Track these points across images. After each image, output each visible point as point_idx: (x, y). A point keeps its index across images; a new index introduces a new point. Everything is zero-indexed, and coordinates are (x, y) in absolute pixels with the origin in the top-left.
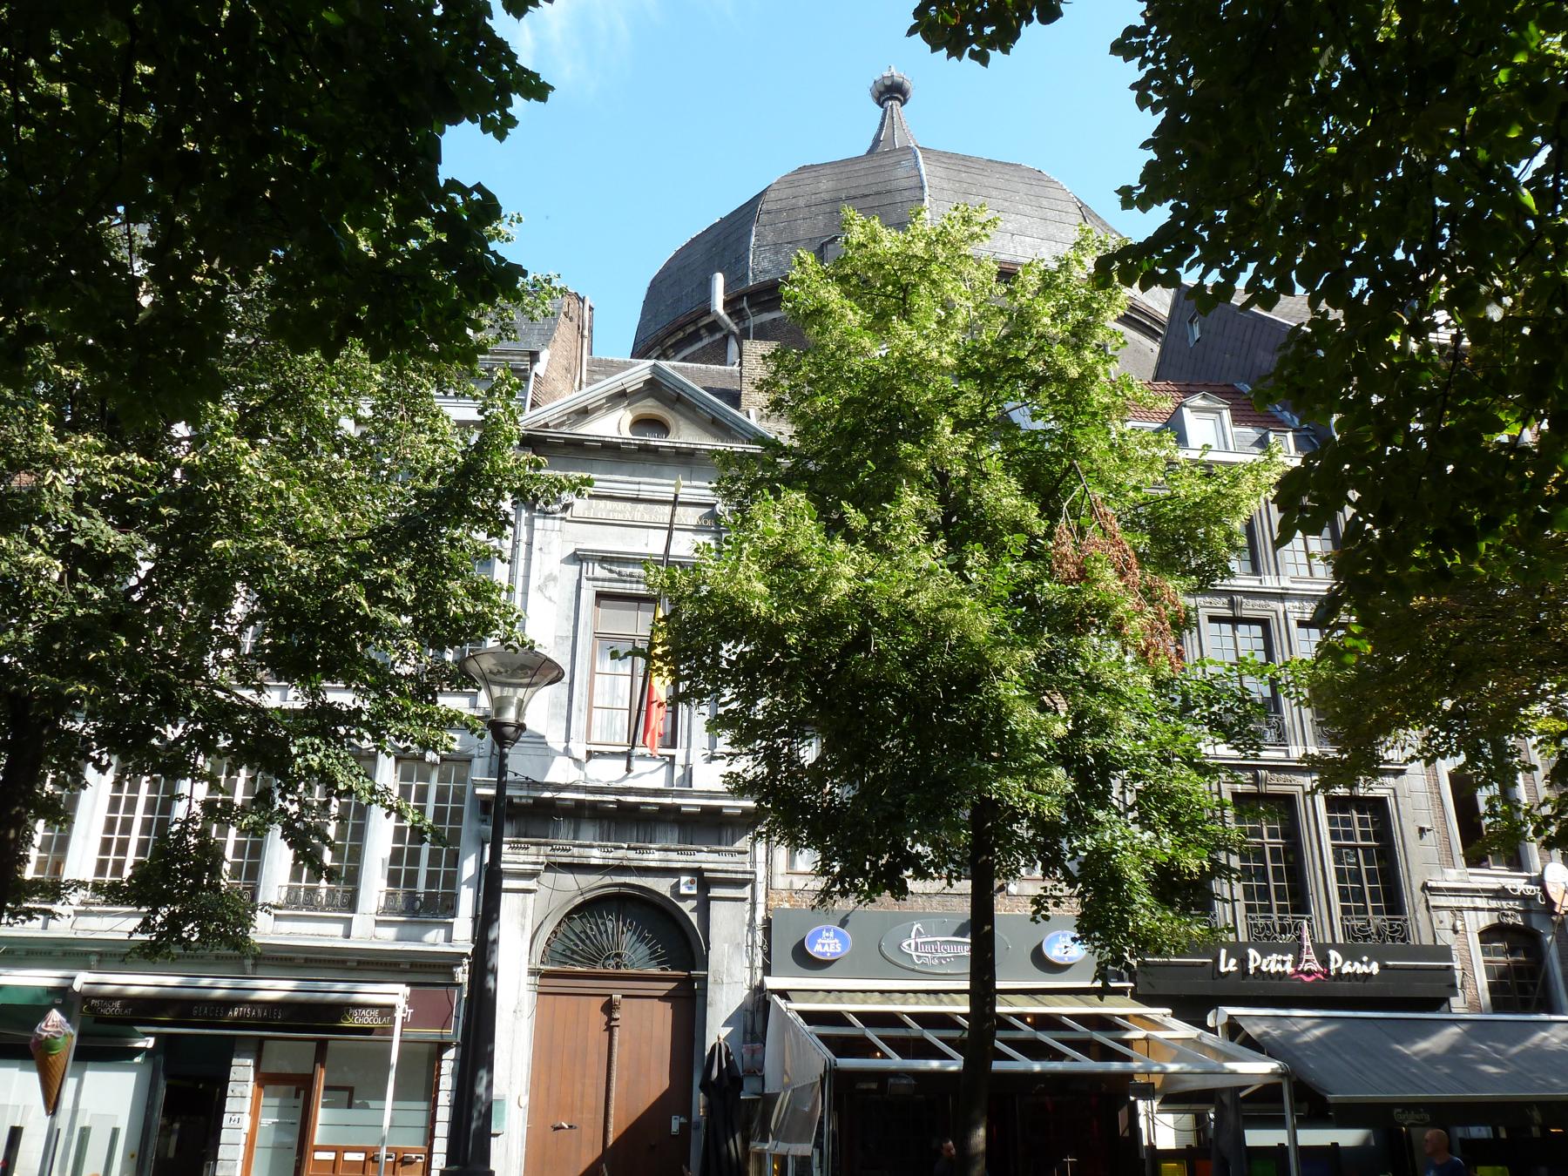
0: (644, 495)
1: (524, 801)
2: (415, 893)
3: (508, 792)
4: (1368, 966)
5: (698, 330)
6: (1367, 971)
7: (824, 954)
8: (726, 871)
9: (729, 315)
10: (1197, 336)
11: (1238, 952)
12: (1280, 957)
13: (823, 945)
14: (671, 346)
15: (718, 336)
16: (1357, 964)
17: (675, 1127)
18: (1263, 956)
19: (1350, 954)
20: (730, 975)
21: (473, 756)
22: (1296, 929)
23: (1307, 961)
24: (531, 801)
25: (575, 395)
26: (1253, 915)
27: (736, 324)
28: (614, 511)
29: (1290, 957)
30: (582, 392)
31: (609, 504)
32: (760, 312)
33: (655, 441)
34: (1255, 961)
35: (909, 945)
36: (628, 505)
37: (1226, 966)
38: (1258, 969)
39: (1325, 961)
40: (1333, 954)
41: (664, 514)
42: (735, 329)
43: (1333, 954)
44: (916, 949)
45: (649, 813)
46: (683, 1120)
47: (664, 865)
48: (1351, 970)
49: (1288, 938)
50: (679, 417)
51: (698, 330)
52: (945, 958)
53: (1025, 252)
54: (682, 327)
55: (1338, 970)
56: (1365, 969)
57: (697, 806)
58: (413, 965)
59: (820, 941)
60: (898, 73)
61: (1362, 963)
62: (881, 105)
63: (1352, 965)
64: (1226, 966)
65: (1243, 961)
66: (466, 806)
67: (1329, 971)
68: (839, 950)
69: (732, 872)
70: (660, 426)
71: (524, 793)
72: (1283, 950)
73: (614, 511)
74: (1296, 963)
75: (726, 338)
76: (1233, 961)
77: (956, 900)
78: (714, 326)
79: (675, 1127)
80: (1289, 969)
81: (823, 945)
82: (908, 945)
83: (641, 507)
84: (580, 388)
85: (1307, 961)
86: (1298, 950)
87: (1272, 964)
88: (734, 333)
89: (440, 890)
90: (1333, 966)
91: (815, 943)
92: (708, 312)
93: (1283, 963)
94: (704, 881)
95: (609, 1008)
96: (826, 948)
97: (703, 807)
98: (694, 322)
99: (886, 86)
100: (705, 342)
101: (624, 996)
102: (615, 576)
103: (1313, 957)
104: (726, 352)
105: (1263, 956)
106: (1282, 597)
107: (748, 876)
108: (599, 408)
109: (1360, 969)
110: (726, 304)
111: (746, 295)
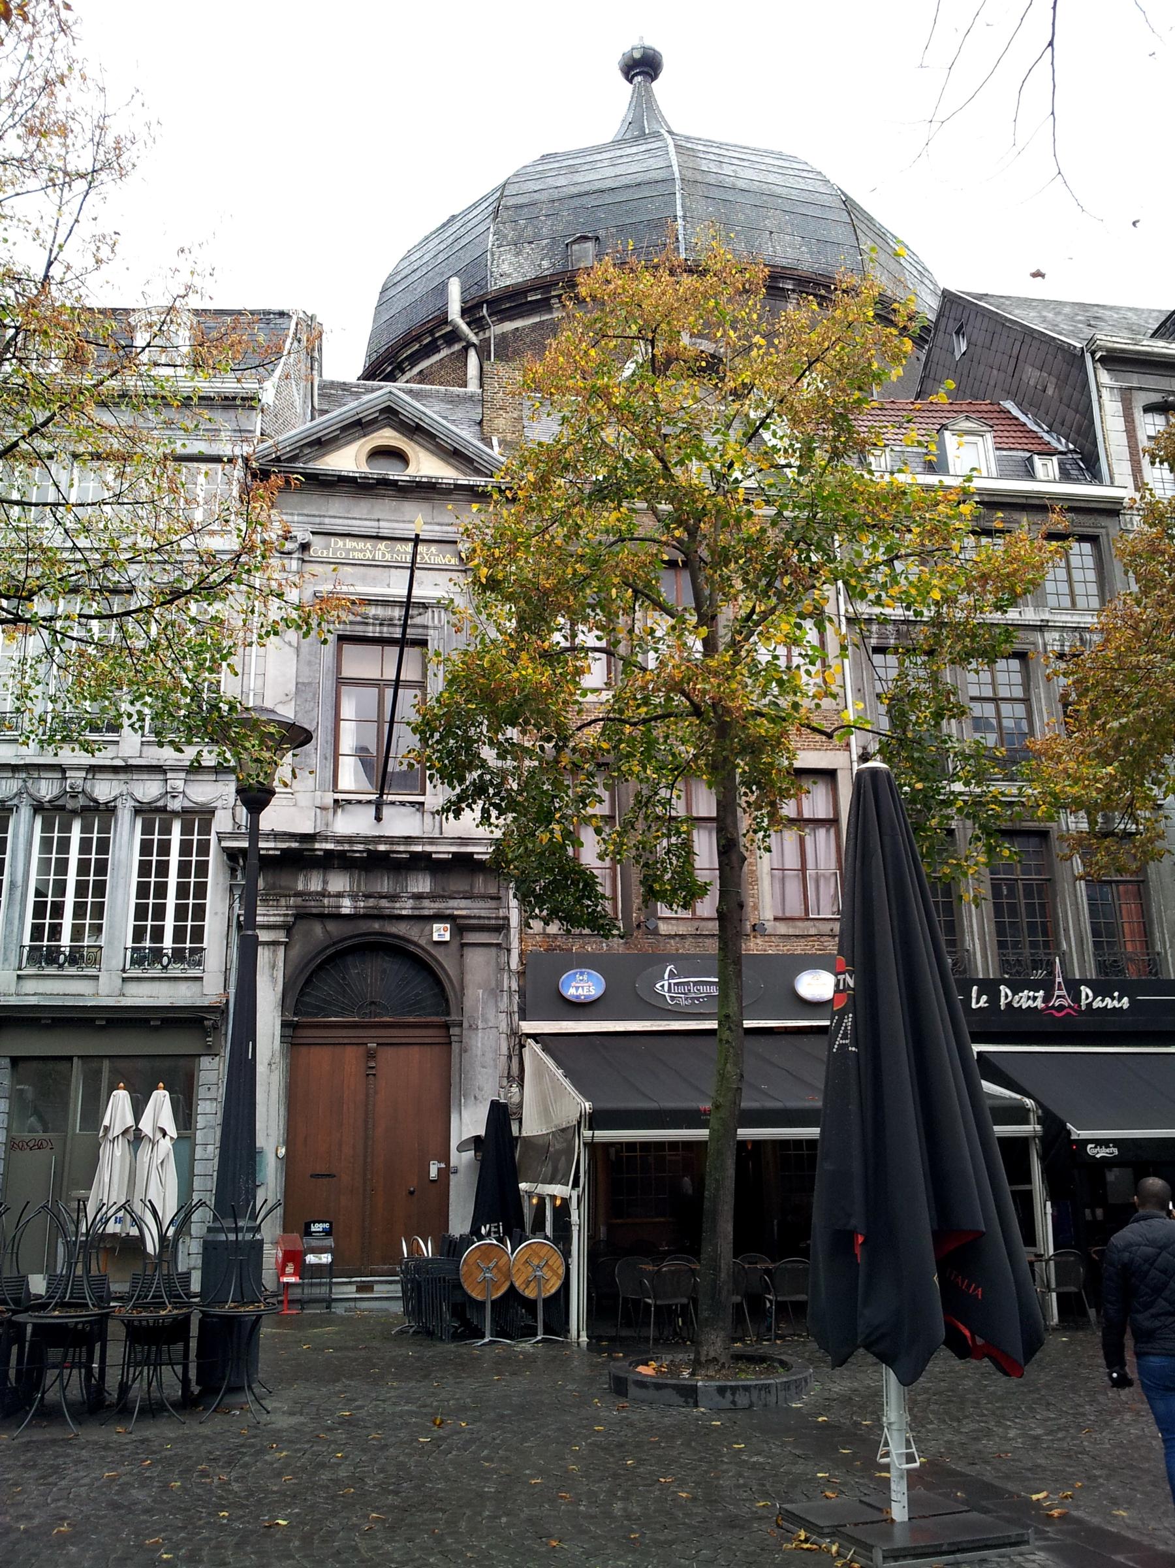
0: (385, 532)
1: (271, 852)
2: (162, 949)
3: (261, 845)
4: (1119, 1001)
5: (435, 340)
6: (1117, 1006)
7: (578, 997)
8: (480, 918)
9: (469, 324)
10: (964, 349)
11: (990, 987)
12: (1031, 994)
13: (577, 988)
14: (406, 358)
15: (457, 347)
16: (1108, 1000)
17: (433, 1173)
18: (1015, 993)
19: (1101, 990)
20: (485, 1020)
21: (216, 808)
22: (1047, 964)
23: (1059, 997)
24: (278, 853)
25: (309, 425)
26: (1004, 951)
27: (476, 334)
28: (354, 549)
29: (1041, 993)
30: (315, 423)
31: (350, 543)
32: (501, 321)
33: (395, 473)
34: (1007, 996)
35: (662, 986)
36: (369, 544)
37: (978, 1002)
38: (1009, 1005)
39: (1076, 997)
40: (1085, 990)
41: (406, 553)
42: (474, 339)
43: (1085, 990)
44: (669, 991)
45: (481, 862)
46: (443, 1165)
47: (417, 913)
48: (1101, 1005)
49: (1040, 974)
50: (418, 448)
51: (435, 340)
52: (698, 999)
53: (785, 252)
54: (417, 338)
55: (1089, 1005)
56: (1116, 1004)
57: (449, 853)
58: (165, 1021)
59: (574, 984)
60: (654, 42)
61: (1113, 998)
62: (631, 82)
63: (1103, 1001)
64: (978, 1002)
65: (994, 997)
66: (212, 858)
67: (1080, 1006)
68: (593, 992)
69: (484, 918)
70: (398, 456)
71: (272, 845)
72: (1034, 986)
73: (354, 549)
74: (1046, 1000)
75: (465, 349)
76: (984, 998)
77: (708, 941)
78: (453, 336)
79: (433, 1173)
80: (1039, 1004)
81: (577, 988)
82: (663, 986)
83: (382, 545)
84: (313, 419)
85: (1059, 997)
86: (1047, 986)
87: (1026, 1000)
88: (474, 345)
89: (188, 945)
90: (1083, 1002)
91: (569, 986)
92: (445, 321)
93: (1035, 998)
94: (460, 927)
95: (371, 1055)
96: (580, 991)
97: (454, 854)
98: (431, 332)
99: (634, 60)
100: (444, 353)
101: (378, 1044)
102: (359, 619)
103: (1064, 992)
104: (466, 365)
105: (1015, 993)
106: (1042, 628)
107: (501, 922)
108: (336, 438)
109: (1109, 1003)
110: (464, 312)
111: (486, 301)
